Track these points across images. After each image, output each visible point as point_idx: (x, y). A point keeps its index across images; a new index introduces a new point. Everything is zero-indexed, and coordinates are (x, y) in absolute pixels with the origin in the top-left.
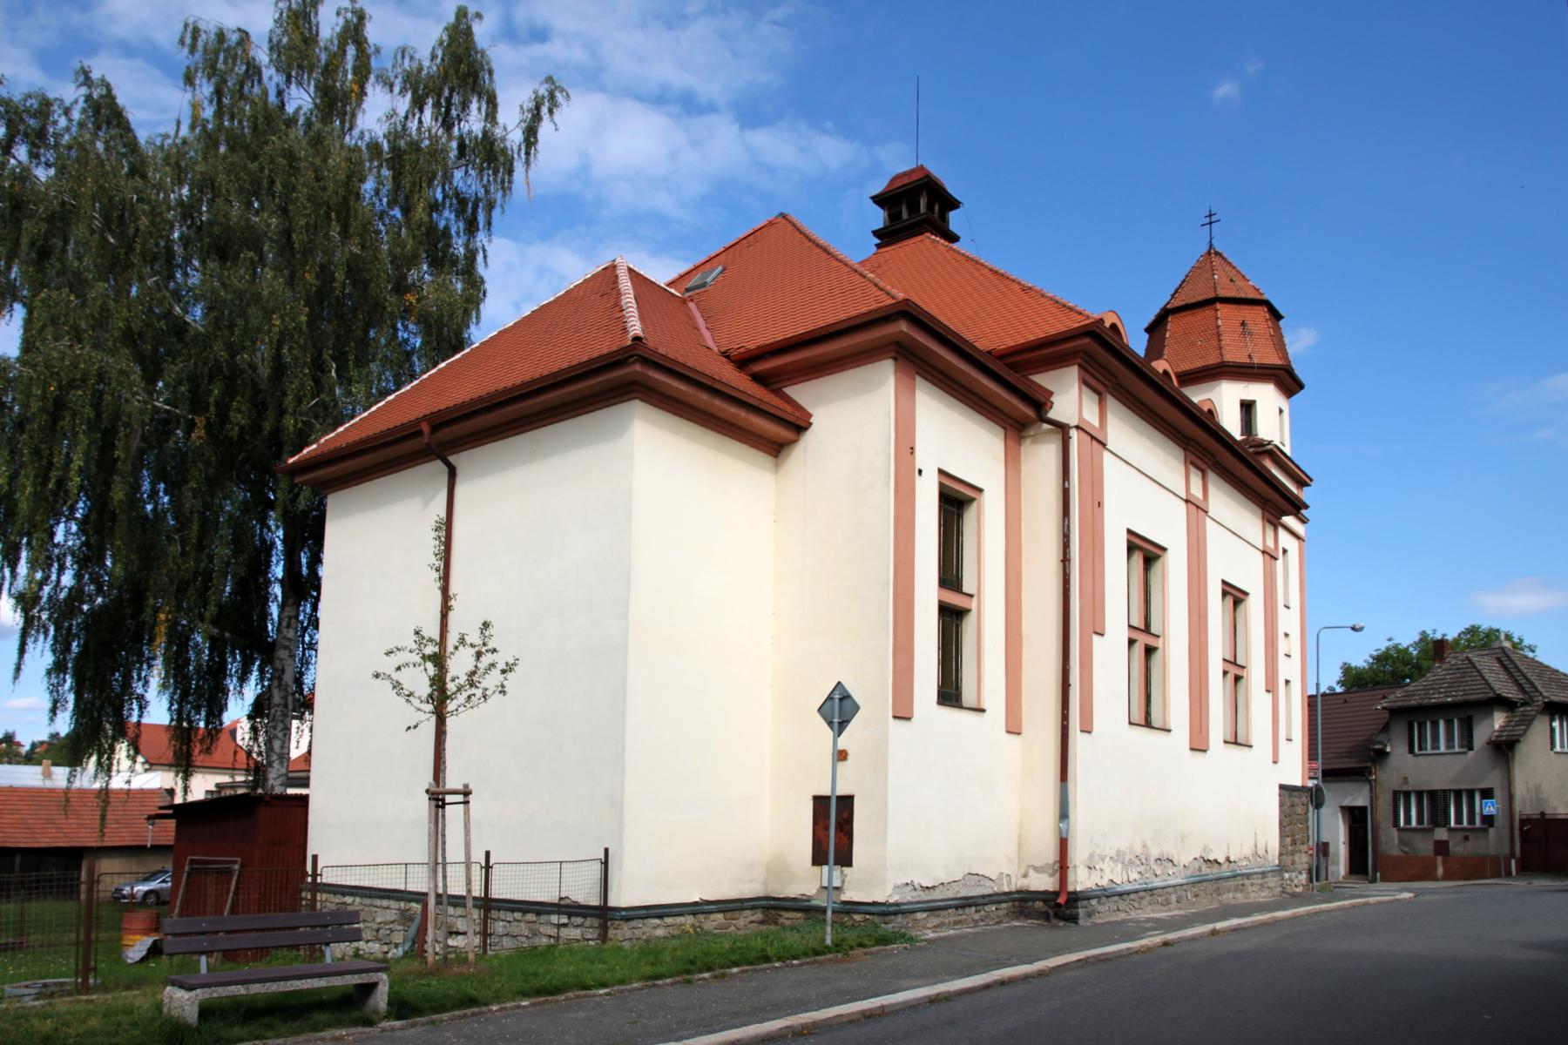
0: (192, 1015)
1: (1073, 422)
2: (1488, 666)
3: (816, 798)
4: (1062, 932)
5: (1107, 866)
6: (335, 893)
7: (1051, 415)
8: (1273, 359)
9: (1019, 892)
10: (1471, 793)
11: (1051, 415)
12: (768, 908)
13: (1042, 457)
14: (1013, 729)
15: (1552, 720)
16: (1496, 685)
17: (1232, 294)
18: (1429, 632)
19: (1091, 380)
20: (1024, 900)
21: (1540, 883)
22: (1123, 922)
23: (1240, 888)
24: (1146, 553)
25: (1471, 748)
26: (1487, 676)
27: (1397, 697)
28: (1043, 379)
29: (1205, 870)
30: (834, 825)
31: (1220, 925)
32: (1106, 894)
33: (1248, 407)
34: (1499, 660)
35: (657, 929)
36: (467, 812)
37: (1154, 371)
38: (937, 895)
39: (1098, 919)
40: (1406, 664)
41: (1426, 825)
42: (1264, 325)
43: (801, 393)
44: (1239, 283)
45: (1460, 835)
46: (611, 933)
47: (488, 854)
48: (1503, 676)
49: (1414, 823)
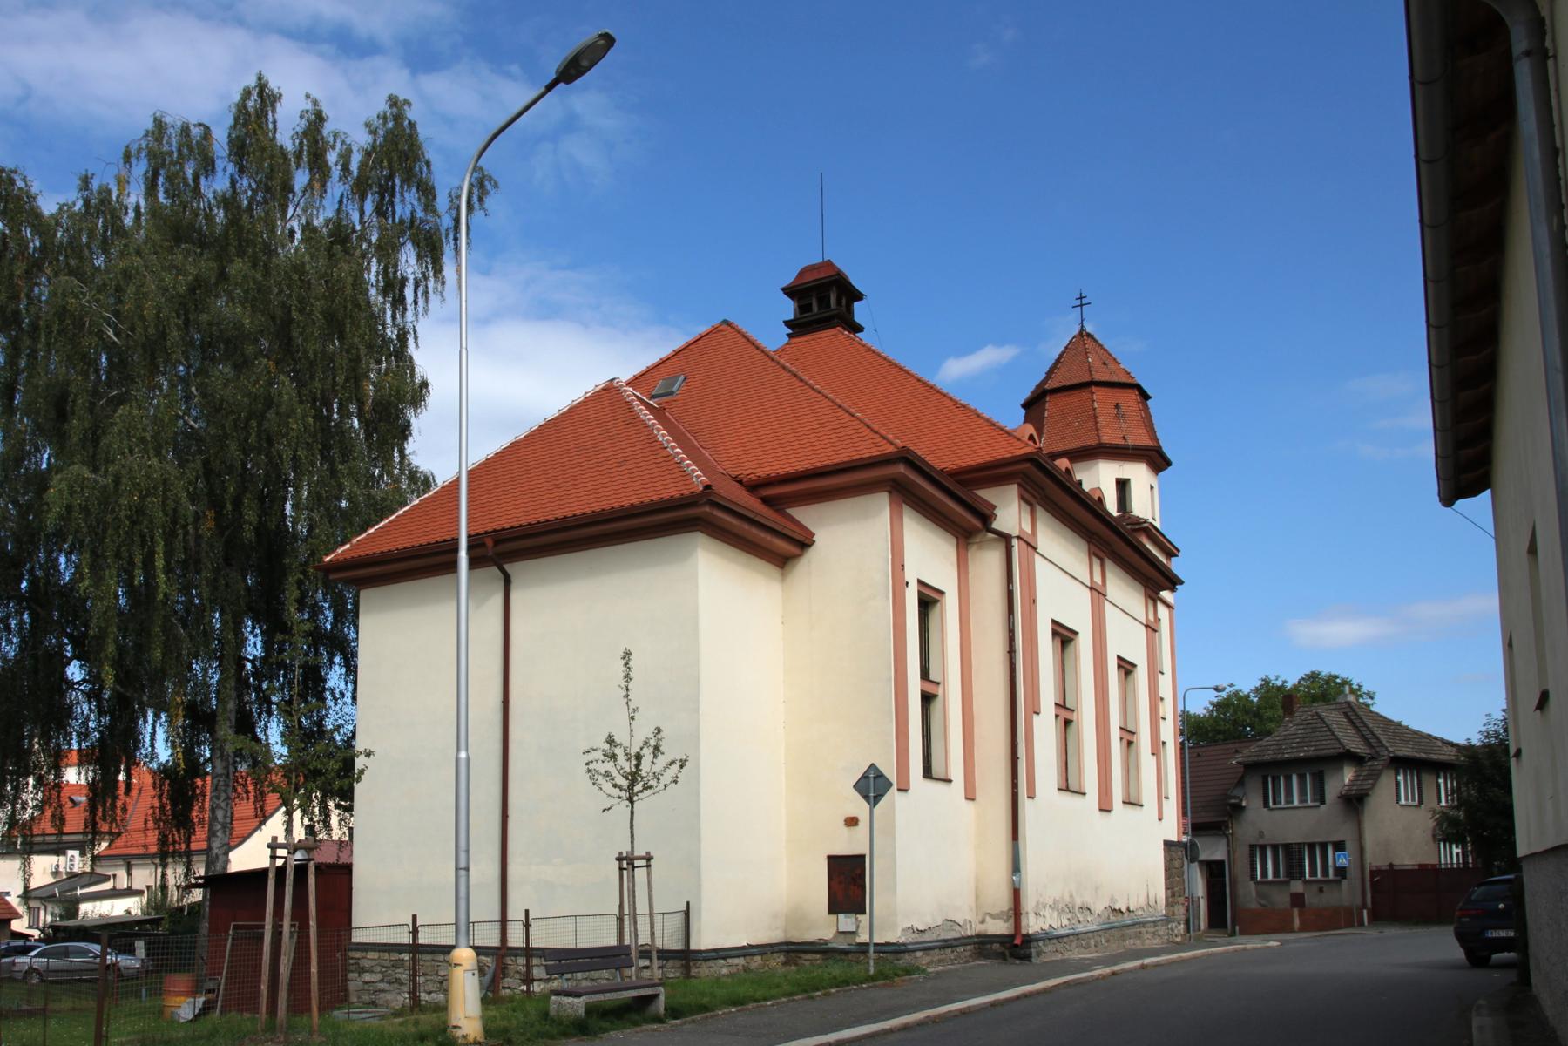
0: (582, 1011)
1: (1015, 533)
2: (1335, 720)
3: (834, 861)
4: (1016, 968)
5: (1047, 912)
6: (389, 952)
7: (995, 525)
8: (1146, 441)
9: (978, 936)
10: (1324, 846)
11: (995, 525)
12: (788, 952)
13: (988, 562)
14: (970, 797)
15: (1397, 774)
16: (1345, 741)
17: (1105, 378)
18: (1272, 678)
19: (1027, 496)
20: (982, 943)
21: (1392, 932)
22: (1063, 961)
23: (1138, 936)
24: (1064, 636)
25: (1323, 802)
26: (1336, 731)
27: (1250, 752)
28: (987, 494)
29: (1113, 918)
30: (848, 881)
31: (1147, 961)
32: (1048, 937)
33: (1123, 485)
34: (1346, 715)
35: (722, 968)
36: (649, 874)
37: (1058, 469)
38: (927, 937)
39: (1045, 958)
40: (1246, 712)
41: (1282, 878)
42: (1135, 408)
43: (805, 515)
44: (1112, 366)
45: (1315, 888)
46: (694, 972)
47: (527, 912)
48: (1351, 731)
49: (1270, 876)
